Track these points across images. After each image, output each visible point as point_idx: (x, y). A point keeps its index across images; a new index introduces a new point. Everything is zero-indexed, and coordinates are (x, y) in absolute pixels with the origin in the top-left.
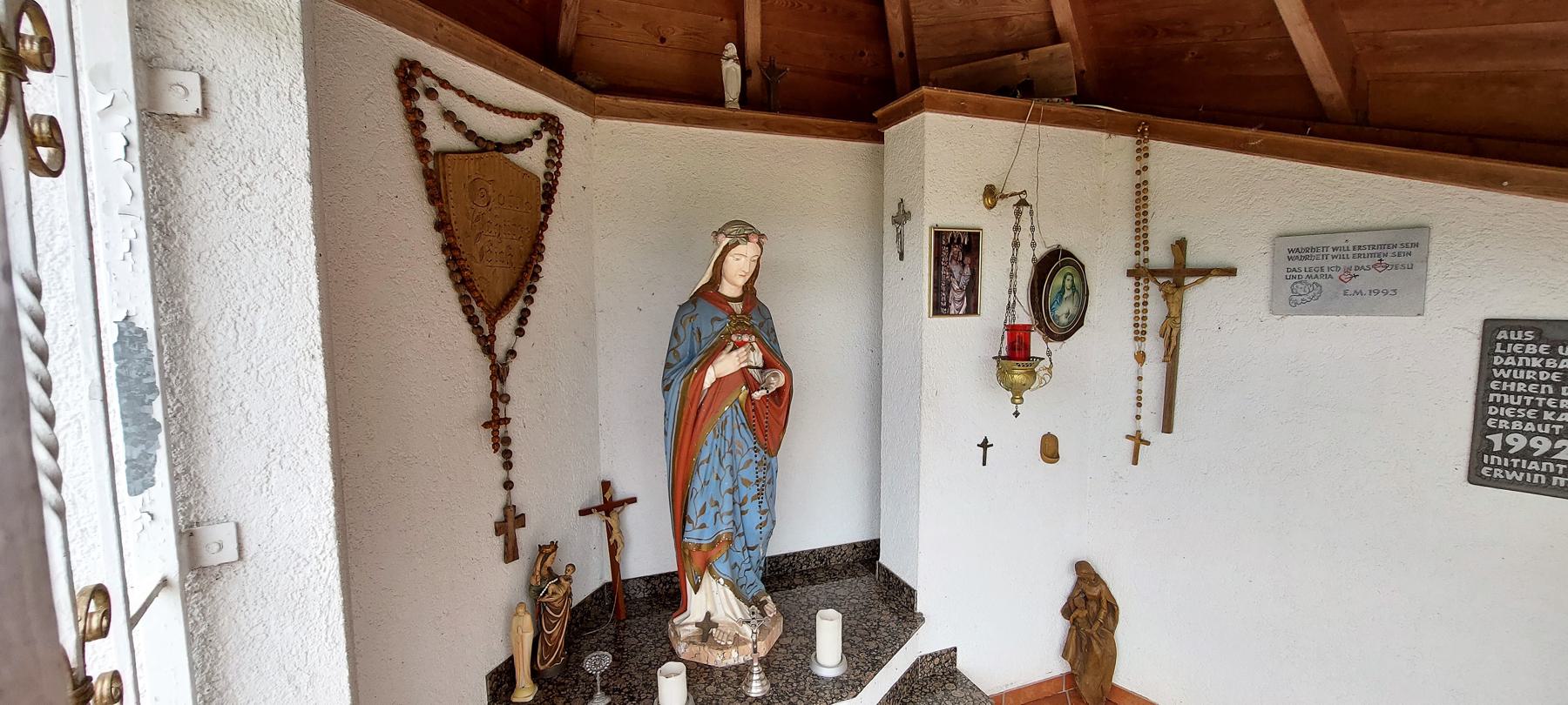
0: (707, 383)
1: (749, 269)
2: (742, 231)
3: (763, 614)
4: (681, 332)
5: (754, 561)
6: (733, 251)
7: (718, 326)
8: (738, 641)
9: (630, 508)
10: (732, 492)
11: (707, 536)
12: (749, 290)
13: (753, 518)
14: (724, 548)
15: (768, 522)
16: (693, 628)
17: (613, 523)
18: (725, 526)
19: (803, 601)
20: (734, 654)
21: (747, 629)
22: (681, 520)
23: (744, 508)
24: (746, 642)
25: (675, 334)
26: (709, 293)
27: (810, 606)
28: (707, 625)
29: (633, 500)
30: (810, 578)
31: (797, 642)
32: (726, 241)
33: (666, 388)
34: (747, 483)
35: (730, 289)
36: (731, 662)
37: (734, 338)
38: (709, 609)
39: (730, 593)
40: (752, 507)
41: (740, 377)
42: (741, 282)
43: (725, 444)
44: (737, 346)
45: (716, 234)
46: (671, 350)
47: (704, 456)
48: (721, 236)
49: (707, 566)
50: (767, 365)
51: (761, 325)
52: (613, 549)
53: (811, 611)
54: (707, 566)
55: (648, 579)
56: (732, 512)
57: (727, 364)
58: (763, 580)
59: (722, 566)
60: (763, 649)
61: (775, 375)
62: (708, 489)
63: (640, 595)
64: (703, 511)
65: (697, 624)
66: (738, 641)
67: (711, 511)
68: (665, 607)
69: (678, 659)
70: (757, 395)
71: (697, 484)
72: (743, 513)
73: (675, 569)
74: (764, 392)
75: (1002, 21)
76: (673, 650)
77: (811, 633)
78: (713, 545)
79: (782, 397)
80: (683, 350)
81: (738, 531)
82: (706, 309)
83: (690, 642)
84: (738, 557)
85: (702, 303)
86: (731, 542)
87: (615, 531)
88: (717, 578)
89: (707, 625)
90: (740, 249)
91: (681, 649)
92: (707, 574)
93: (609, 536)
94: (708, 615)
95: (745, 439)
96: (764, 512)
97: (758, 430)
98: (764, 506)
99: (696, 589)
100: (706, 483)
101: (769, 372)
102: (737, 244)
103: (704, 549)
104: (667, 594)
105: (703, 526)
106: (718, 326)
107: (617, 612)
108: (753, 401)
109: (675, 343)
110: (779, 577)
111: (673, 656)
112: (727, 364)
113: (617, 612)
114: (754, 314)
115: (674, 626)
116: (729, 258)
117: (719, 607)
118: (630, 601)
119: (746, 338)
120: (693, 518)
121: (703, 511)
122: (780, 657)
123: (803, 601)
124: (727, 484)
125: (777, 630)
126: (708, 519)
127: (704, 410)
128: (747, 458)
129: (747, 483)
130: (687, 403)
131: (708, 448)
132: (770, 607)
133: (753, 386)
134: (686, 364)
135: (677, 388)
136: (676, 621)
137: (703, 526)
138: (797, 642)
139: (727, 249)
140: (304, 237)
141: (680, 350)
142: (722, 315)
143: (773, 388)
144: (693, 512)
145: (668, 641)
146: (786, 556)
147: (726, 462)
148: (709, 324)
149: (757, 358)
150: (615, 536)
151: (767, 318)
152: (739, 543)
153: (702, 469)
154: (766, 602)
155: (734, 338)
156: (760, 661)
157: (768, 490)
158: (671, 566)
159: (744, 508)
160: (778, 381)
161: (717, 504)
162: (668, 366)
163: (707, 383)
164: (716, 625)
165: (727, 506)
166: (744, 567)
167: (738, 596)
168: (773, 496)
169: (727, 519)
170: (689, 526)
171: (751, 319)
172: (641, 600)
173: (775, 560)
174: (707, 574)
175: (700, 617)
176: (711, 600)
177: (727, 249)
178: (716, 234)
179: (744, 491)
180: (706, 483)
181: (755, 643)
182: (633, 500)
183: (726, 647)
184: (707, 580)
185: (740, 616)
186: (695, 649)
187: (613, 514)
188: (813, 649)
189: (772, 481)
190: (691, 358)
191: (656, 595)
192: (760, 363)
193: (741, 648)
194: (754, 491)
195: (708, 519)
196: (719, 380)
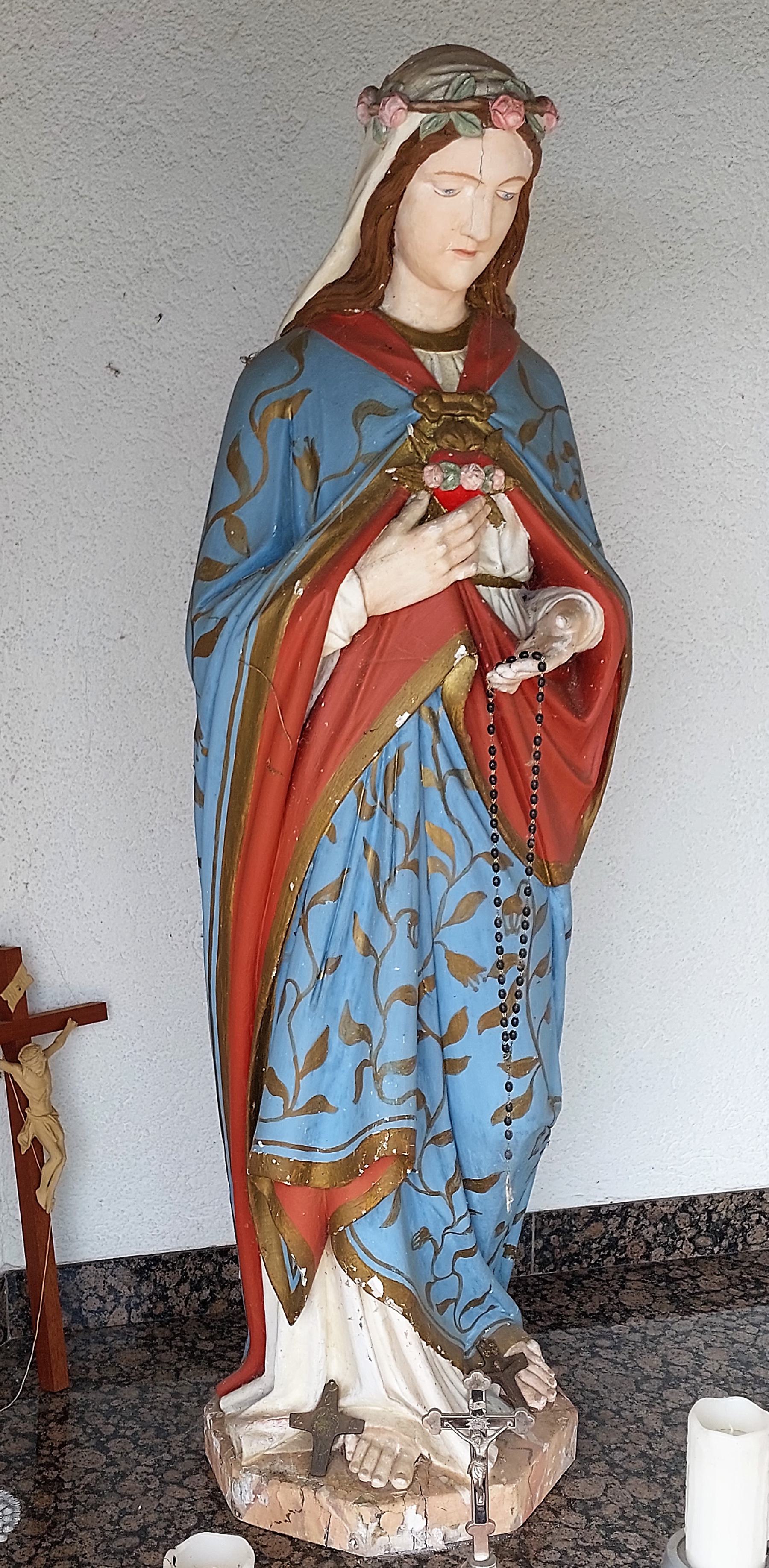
0: (339, 632)
1: (488, 226)
2: (469, 85)
3: (513, 1398)
4: (251, 453)
5: (487, 1226)
6: (434, 162)
7: (376, 435)
8: (426, 1479)
9: (85, 1039)
10: (416, 995)
11: (332, 1136)
12: (488, 308)
13: (482, 1086)
14: (387, 1179)
15: (536, 1104)
16: (283, 1431)
17: (28, 1079)
18: (388, 1106)
19: (650, 1363)
20: (414, 1520)
21: (455, 1448)
22: (246, 1083)
23: (455, 1051)
24: (451, 1485)
25: (231, 459)
26: (348, 316)
27: (670, 1381)
28: (328, 1424)
29: (96, 1012)
30: (677, 1289)
31: (622, 1495)
32: (407, 124)
33: (201, 647)
34: (465, 969)
35: (423, 299)
36: (402, 1544)
37: (432, 477)
38: (335, 1374)
39: (403, 1326)
40: (481, 1048)
41: (449, 613)
42: (461, 274)
43: (401, 813)
44: (447, 502)
45: (376, 96)
46: (218, 515)
47: (326, 874)
48: (393, 107)
49: (329, 1233)
50: (544, 573)
51: (527, 432)
52: (29, 1168)
53: (673, 1398)
54: (329, 1233)
55: (145, 1267)
56: (415, 1064)
57: (406, 569)
58: (518, 1288)
59: (378, 1238)
60: (507, 1510)
61: (571, 610)
62: (341, 986)
63: (120, 1317)
64: (319, 1054)
65: (295, 1419)
66: (426, 1479)
67: (344, 1056)
68: (195, 1356)
69: (231, 1525)
70: (506, 677)
71: (302, 968)
72: (450, 1067)
73: (229, 1238)
74: (527, 668)
75: (39, 1010)
76: (216, 1496)
77: (668, 1472)
78: (348, 1170)
79: (593, 684)
80: (257, 514)
81: (432, 1122)
82: (336, 369)
83: (271, 1472)
84: (432, 1212)
85: (322, 350)
86: (407, 1160)
87: (35, 1110)
88: (358, 1274)
89: (328, 1424)
90: (458, 154)
91: (243, 1493)
92: (327, 1262)
93: (17, 1123)
94: (332, 1391)
95: (461, 822)
96: (519, 1068)
97: (505, 786)
98: (522, 1049)
99: (294, 1307)
100: (330, 965)
101: (549, 599)
102: (448, 134)
103: (320, 1179)
104: (201, 1316)
105: (318, 1105)
106: (376, 435)
107: (41, 1366)
108: (494, 701)
109: (232, 493)
110: (573, 1283)
111: (219, 1516)
112: (406, 569)
113: (41, 1366)
114: (503, 391)
115: (221, 1420)
116: (421, 188)
117: (368, 1370)
118: (78, 1330)
119: (471, 479)
120: (286, 1075)
121: (319, 1054)
122: (562, 1540)
123: (650, 1363)
124: (398, 969)
125: (557, 1453)
126: (336, 1080)
127: (325, 724)
128: (465, 886)
129: (465, 969)
130: (271, 699)
131: (338, 848)
132: (538, 1380)
133: (492, 644)
134: (270, 564)
135: (236, 649)
136: (228, 1403)
137: (318, 1105)
138: (622, 1495)
139: (413, 154)
140: (763, 331)
141: (248, 515)
142: (393, 394)
143: (560, 655)
144: (286, 1057)
145: (203, 1464)
146: (596, 1213)
147: (398, 899)
148: (354, 425)
149: (508, 549)
150: (36, 1124)
151: (548, 407)
152: (436, 1166)
153: (319, 918)
154: (521, 1361)
155: (432, 477)
156: (498, 1546)
157: (535, 994)
158: (217, 1230)
159: (455, 1051)
160: (578, 628)
161: (364, 1034)
162: (206, 570)
163: (339, 632)
164: (357, 1426)
165: (396, 1041)
166: (452, 1244)
167: (429, 1333)
168: (552, 1015)
169: (396, 1085)
170: (271, 1105)
171: (488, 397)
172: (122, 1331)
173: (562, 1221)
174: (327, 1262)
175: (306, 1398)
176: (340, 1343)
177: (413, 154)
178: (376, 96)
179: (455, 995)
180: (330, 965)
181: (480, 1489)
182: (96, 1012)
183: (388, 1495)
184: (329, 1279)
185: (434, 1400)
186: (286, 1495)
187: (30, 1057)
188: (674, 1521)
189: (550, 967)
190: (286, 543)
191: (168, 1319)
192: (521, 569)
193: (436, 1502)
194: (486, 997)
195: (336, 1080)
196: (377, 624)
